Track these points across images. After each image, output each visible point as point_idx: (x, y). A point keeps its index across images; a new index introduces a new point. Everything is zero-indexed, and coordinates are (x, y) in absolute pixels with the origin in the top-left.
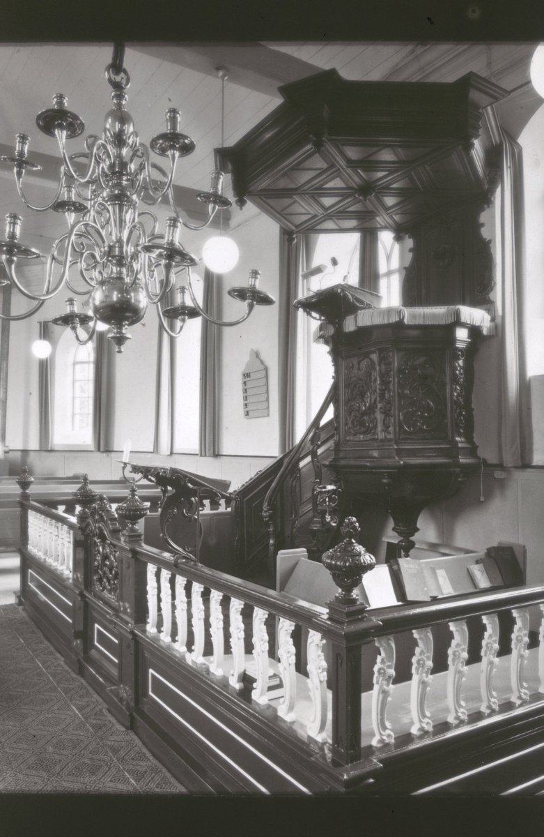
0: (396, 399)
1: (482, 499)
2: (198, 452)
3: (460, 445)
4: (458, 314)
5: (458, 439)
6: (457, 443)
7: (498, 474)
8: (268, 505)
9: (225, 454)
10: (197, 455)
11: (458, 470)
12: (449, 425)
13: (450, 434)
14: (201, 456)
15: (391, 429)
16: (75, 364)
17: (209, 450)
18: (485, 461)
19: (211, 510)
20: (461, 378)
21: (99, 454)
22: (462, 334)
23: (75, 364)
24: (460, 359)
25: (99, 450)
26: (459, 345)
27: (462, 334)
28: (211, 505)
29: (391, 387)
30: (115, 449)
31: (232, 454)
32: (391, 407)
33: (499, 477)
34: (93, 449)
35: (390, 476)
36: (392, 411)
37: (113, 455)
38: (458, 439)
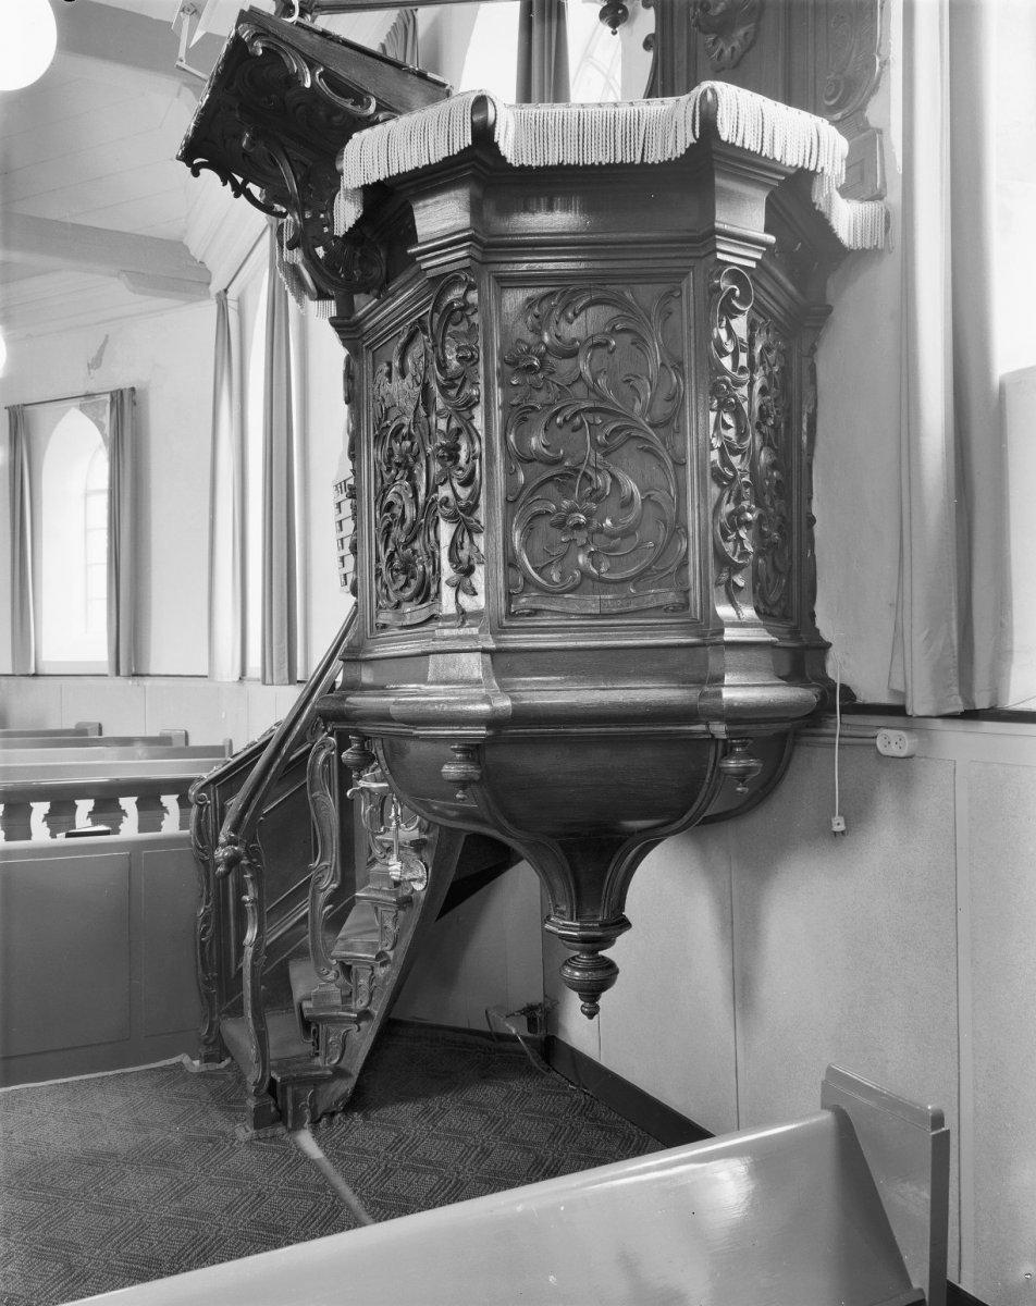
0: (499, 466)
1: (838, 824)
2: (106, 669)
3: (730, 635)
4: (707, 121)
5: (725, 611)
6: (720, 626)
7: (892, 741)
8: (235, 829)
9: (47, 672)
10: (106, 675)
11: (719, 729)
12: (694, 559)
13: (695, 596)
14: (264, 683)
15: (478, 578)
16: (86, 495)
17: (280, 669)
18: (847, 692)
19: (140, 831)
20: (739, 384)
21: (120, 682)
22: (745, 218)
23: (86, 495)
24: (732, 313)
25: (118, 674)
26: (729, 254)
27: (745, 218)
28: (139, 810)
29: (479, 422)
30: (151, 672)
31: (185, 674)
32: (475, 496)
33: (894, 750)
34: (106, 672)
35: (472, 751)
36: (481, 514)
37: (148, 682)
38: (725, 611)
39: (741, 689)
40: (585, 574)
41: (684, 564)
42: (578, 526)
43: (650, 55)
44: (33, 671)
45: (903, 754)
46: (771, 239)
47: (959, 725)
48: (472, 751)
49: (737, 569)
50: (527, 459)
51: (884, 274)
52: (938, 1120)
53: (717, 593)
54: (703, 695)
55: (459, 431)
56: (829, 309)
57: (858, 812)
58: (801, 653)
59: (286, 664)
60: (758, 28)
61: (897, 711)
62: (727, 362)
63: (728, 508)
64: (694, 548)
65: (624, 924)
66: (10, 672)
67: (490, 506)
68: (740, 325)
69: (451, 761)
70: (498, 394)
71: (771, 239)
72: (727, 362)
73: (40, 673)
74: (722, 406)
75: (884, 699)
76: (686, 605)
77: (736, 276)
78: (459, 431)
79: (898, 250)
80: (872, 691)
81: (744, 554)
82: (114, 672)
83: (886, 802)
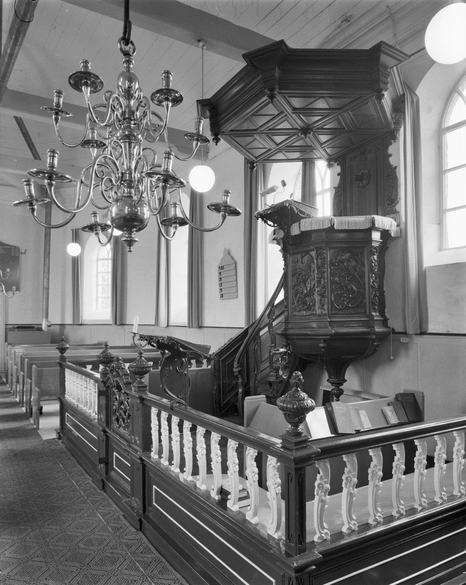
1: (392, 358)
2: (187, 325)
5: (374, 314)
6: (373, 317)
7: (403, 339)
8: (238, 364)
9: (85, 323)
12: (367, 303)
13: (368, 310)
14: (189, 327)
15: (326, 307)
16: (98, 260)
19: (197, 367)
21: (116, 327)
22: (376, 236)
23: (98, 260)
25: (116, 324)
27: (376, 236)
30: (127, 323)
33: (404, 341)
34: (111, 323)
35: (325, 341)
36: (326, 294)
37: (126, 327)
38: (374, 314)
39: (378, 329)
40: (346, 306)
41: (365, 304)
42: (345, 296)
43: (339, 177)
44: (80, 323)
45: (407, 342)
46: (382, 241)
47: (419, 336)
48: (325, 341)
49: (376, 305)
50: (336, 283)
51: (400, 242)
52: (423, 393)
53: (372, 310)
54: (371, 330)
55: (321, 278)
56: (388, 247)
57: (396, 355)
58: (385, 322)
59: (197, 321)
60: (369, 182)
61: (405, 333)
62: (373, 264)
63: (374, 293)
64: (367, 301)
65: (345, 381)
66: (72, 323)
67: (328, 292)
68: (375, 257)
69: (321, 343)
70: (329, 270)
71: (382, 241)
72: (373, 264)
73: (82, 323)
74: (373, 273)
75: (402, 331)
76: (366, 312)
77: (375, 248)
78: (321, 278)
79: (404, 236)
80: (399, 328)
81: (377, 302)
82: (114, 323)
83: (403, 352)
